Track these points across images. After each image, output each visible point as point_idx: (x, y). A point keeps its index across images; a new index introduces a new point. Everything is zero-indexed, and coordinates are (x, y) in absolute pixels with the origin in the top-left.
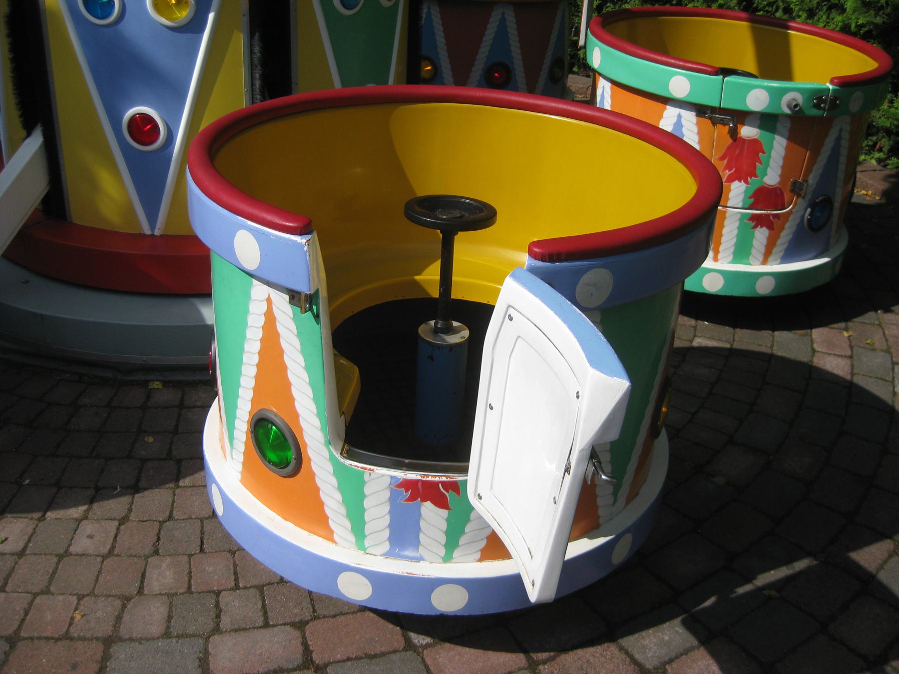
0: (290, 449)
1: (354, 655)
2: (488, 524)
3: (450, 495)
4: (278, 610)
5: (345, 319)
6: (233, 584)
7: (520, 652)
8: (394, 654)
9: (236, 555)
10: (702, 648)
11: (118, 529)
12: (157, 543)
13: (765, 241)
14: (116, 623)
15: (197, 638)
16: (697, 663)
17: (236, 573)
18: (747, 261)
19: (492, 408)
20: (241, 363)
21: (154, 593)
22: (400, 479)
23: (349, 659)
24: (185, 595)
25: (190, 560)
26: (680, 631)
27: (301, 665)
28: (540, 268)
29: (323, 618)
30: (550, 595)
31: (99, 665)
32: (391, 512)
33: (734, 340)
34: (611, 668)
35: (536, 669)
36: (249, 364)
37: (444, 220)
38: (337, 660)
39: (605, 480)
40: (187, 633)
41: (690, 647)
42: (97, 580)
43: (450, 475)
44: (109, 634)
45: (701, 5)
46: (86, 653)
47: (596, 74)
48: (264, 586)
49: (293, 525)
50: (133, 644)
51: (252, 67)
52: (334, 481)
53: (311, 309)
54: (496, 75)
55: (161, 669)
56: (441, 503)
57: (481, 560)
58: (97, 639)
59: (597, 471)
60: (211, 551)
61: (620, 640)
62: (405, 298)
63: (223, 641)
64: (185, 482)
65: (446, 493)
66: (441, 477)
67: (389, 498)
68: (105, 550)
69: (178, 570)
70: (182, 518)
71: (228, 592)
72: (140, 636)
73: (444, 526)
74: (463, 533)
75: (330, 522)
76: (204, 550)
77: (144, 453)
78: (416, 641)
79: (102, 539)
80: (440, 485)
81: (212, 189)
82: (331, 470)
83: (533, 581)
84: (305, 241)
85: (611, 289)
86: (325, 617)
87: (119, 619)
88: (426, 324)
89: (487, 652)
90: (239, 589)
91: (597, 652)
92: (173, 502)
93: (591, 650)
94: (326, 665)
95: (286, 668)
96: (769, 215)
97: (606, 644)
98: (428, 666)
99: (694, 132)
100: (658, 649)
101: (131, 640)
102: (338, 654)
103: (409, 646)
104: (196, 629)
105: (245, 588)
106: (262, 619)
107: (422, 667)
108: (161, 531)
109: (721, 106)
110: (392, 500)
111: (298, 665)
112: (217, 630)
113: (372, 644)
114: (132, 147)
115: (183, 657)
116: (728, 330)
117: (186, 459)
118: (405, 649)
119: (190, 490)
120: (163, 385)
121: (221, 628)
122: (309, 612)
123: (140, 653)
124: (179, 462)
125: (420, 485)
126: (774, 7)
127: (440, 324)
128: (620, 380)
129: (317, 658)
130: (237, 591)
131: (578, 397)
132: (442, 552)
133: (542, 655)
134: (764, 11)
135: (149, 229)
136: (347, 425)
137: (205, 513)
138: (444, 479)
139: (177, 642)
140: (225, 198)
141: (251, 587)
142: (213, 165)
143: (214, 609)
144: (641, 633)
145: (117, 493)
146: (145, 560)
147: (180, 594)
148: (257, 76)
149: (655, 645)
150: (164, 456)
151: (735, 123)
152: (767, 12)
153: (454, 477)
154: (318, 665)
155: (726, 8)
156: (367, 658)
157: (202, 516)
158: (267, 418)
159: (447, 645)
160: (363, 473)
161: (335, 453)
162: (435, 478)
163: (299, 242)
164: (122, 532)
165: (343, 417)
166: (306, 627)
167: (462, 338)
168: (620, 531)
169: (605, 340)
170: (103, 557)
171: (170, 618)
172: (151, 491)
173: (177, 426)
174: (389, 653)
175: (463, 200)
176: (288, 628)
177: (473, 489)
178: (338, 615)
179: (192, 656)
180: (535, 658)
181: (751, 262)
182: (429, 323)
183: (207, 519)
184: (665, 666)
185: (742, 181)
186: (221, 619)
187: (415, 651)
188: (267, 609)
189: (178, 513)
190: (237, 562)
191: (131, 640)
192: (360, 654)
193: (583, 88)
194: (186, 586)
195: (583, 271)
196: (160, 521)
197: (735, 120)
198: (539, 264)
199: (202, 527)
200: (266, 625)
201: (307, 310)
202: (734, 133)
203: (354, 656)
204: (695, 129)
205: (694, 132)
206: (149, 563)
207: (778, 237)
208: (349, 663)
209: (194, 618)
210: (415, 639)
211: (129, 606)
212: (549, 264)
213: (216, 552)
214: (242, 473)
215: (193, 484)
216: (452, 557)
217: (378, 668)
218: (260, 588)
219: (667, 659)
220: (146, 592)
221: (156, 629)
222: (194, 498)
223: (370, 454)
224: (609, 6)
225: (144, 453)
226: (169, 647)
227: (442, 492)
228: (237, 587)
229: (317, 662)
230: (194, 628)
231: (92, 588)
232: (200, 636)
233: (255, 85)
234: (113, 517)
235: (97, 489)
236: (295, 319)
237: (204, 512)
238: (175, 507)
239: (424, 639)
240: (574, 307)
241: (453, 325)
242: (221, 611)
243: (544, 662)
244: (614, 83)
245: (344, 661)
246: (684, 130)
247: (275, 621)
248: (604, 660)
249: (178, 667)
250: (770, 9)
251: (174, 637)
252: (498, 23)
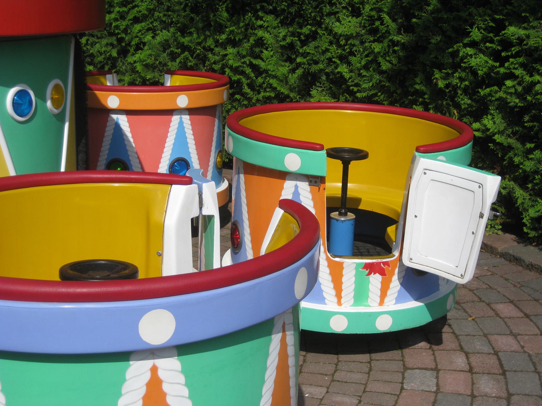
13: (379, 286)
96: (380, 263)
204: (310, 196)
207: (390, 281)
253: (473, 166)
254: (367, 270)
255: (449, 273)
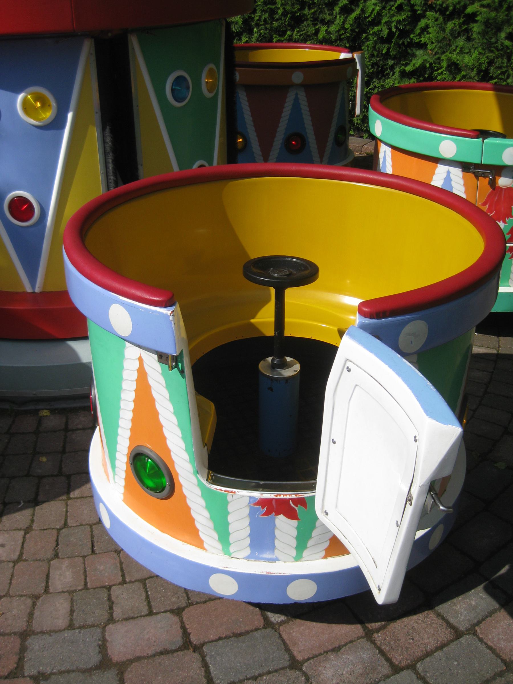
0: (163, 476)
1: (224, 634)
2: (328, 529)
3: (299, 509)
4: (159, 600)
5: (198, 359)
6: (120, 579)
7: (358, 624)
8: (256, 632)
9: (121, 554)
10: (502, 610)
11: (24, 538)
12: (57, 548)
14: (29, 619)
15: (95, 627)
16: (500, 623)
17: (122, 570)
18: (507, 284)
19: (334, 443)
20: (119, 408)
21: (58, 591)
22: (257, 498)
23: (220, 639)
24: (83, 591)
25: (84, 560)
26: (484, 596)
27: (182, 646)
28: (370, 324)
29: (196, 604)
30: (395, 597)
31: (18, 657)
32: (250, 525)
33: (499, 347)
34: (432, 632)
35: (372, 637)
36: (126, 410)
37: (277, 278)
38: (211, 640)
39: (443, 511)
40: (87, 624)
41: (493, 610)
42: (10, 583)
43: (299, 493)
44: (24, 629)
45: (448, 77)
46: (6, 646)
47: (378, 140)
48: (146, 579)
49: (170, 536)
50: (44, 637)
51: (105, 154)
52: (202, 502)
53: (177, 366)
54: (294, 143)
55: (69, 657)
56: (292, 515)
57: (325, 557)
58: (15, 633)
59: (436, 502)
60: (100, 552)
61: (437, 607)
62: (244, 338)
63: (116, 630)
64: (75, 494)
65: (296, 508)
66: (291, 495)
67: (249, 514)
68: (15, 556)
69: (75, 570)
70: (75, 525)
71: (118, 586)
72: (49, 629)
73: (295, 533)
74: (310, 537)
75: (200, 534)
76: (95, 552)
77: (40, 471)
78: (273, 619)
79: (12, 547)
80: (291, 501)
81: (88, 270)
82: (200, 493)
83: (379, 587)
84: (170, 312)
85: (426, 335)
86: (197, 603)
87: (31, 615)
88: (264, 361)
89: (331, 625)
90: (126, 584)
91: (419, 620)
92: (67, 511)
93: (415, 617)
94: (203, 645)
95: (170, 650)
97: (426, 612)
98: (284, 640)
99: (460, 184)
100: (468, 613)
101: (43, 633)
102: (211, 634)
103: (268, 624)
104: (94, 620)
105: (131, 582)
106: (147, 608)
107: (279, 641)
108: (59, 537)
109: (482, 163)
110: (251, 515)
111: (179, 646)
112: (111, 620)
113: (238, 625)
114: (12, 223)
115: (85, 645)
116: (494, 338)
117: (74, 474)
118: (265, 627)
119: (79, 500)
120: (51, 413)
121: (115, 618)
122: (184, 600)
123: (50, 644)
124: (68, 477)
125: (274, 502)
126: (506, 75)
127: (276, 361)
128: (454, 427)
129: (194, 639)
130: (125, 585)
131: (416, 441)
132: (294, 553)
133: (376, 625)
134: (498, 79)
135: (31, 288)
136: (209, 453)
137: (93, 520)
138: (294, 496)
139: (80, 632)
140: (99, 277)
141: (135, 581)
142: (84, 245)
143: (108, 602)
144: (453, 600)
145: (22, 506)
146: (48, 563)
147: (79, 591)
148: (110, 160)
149: (465, 610)
150: (56, 473)
151: (494, 176)
152: (501, 79)
153: (302, 494)
154: (195, 645)
155: (468, 78)
156: (234, 637)
157: (91, 523)
158: (143, 453)
159: (298, 621)
160: (226, 495)
161: (202, 480)
162: (286, 496)
163: (165, 313)
164: (27, 540)
165: (206, 447)
166: (183, 613)
167: (295, 371)
168: (435, 524)
169: (435, 389)
170: (13, 562)
171: (72, 611)
172: (48, 503)
173: (64, 447)
174: (252, 631)
175: (290, 259)
176: (168, 614)
177: (320, 507)
178: (208, 601)
179: (93, 644)
180: (370, 627)
181: (511, 285)
182: (267, 360)
183: (95, 524)
184: (475, 627)
185: (501, 221)
186: (113, 610)
187: (273, 628)
188: (150, 599)
189: (71, 521)
190: (123, 560)
191: (43, 633)
192: (229, 633)
193: (358, 147)
194: (83, 583)
195: (403, 324)
196: (57, 529)
197: (494, 172)
198: (368, 321)
199: (92, 531)
200: (151, 613)
201: (174, 367)
202: (493, 184)
203: (224, 636)
204: (462, 182)
205: (460, 184)
206: (51, 565)
208: (221, 642)
209: (92, 611)
210: (272, 618)
211: (38, 604)
212: (376, 321)
213: (105, 552)
214: (124, 494)
215: (81, 495)
216: (302, 557)
217: (244, 645)
218: (143, 581)
219: (476, 621)
220: (51, 591)
221: (62, 622)
222: (83, 507)
223: (231, 478)
224: (375, 82)
225: (40, 471)
226: (74, 637)
227: (292, 507)
228: (124, 582)
229: (194, 643)
230: (93, 619)
231: (7, 590)
232: (97, 626)
233: (109, 168)
234: (19, 528)
235: (5, 504)
236: (163, 374)
237: (92, 519)
238: (69, 516)
239: (279, 617)
240: (404, 359)
241: (287, 360)
242: (113, 603)
243: (378, 630)
244: (394, 148)
245: (216, 641)
246: (453, 183)
247: (157, 609)
248: (426, 626)
249: (82, 654)
250: (502, 77)
251: (77, 628)
252: (292, 102)
253: (402, 340)
254: (511, 253)
255: (368, 551)
